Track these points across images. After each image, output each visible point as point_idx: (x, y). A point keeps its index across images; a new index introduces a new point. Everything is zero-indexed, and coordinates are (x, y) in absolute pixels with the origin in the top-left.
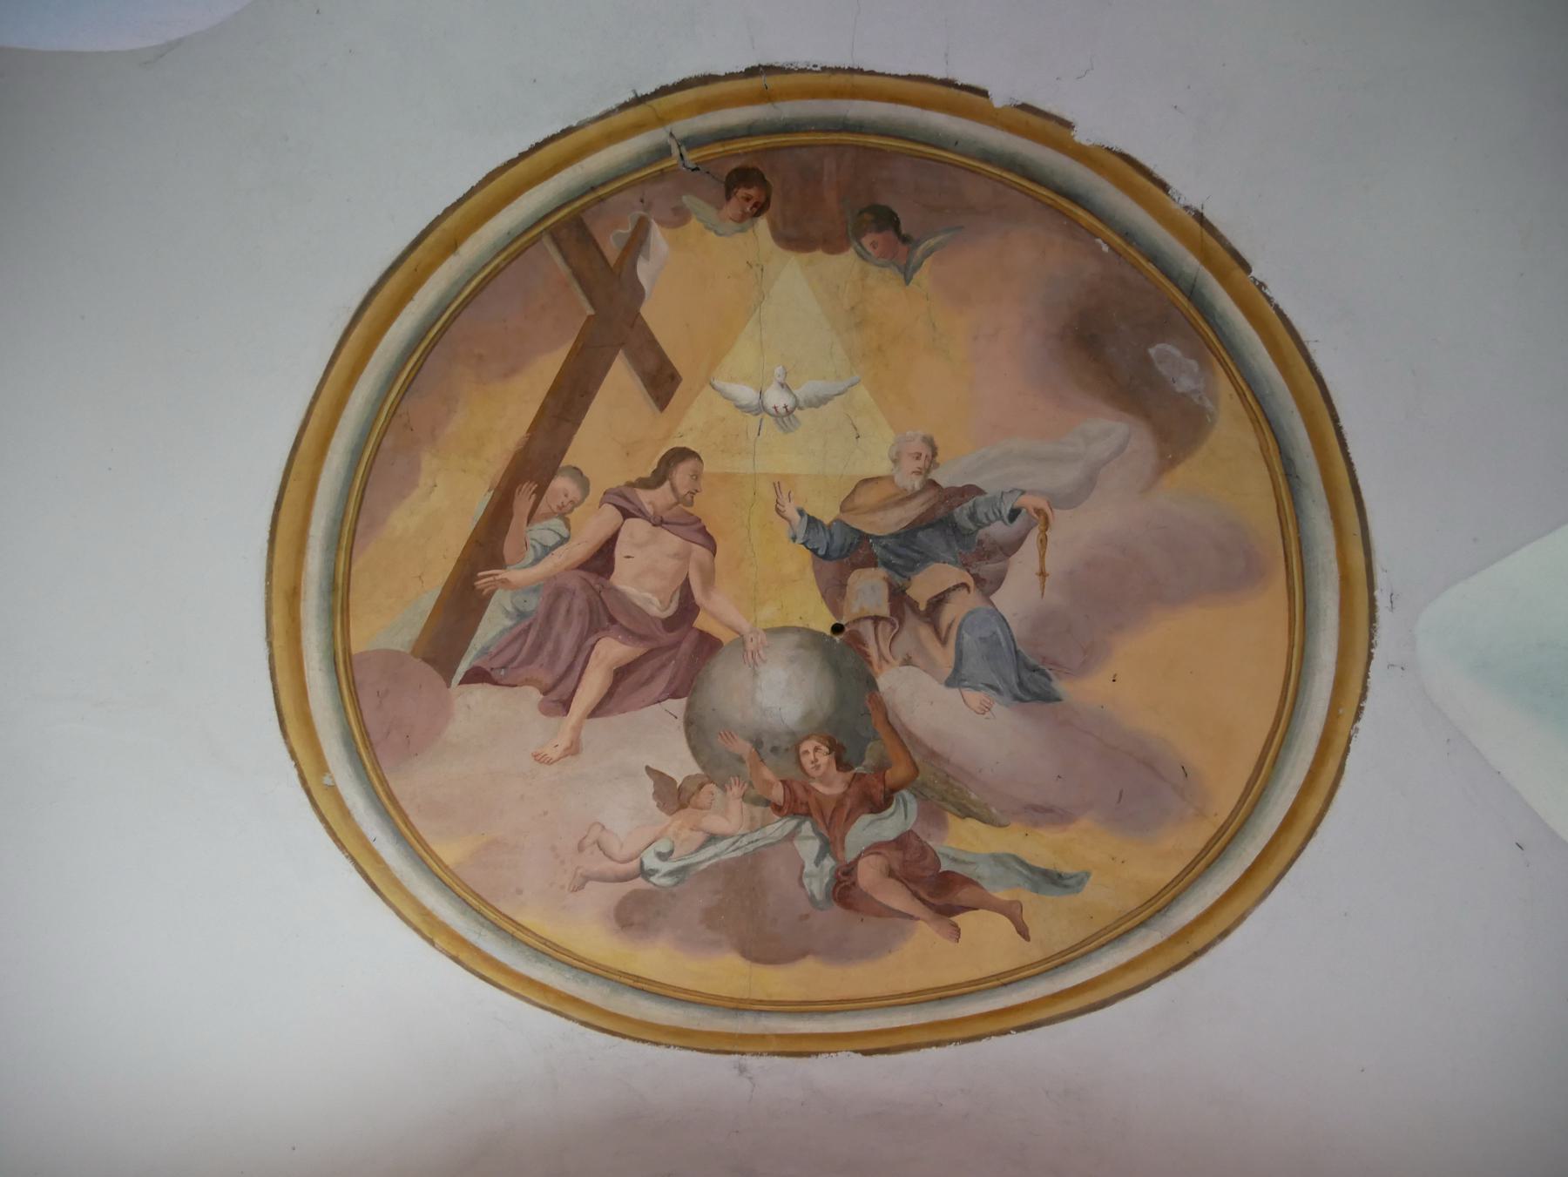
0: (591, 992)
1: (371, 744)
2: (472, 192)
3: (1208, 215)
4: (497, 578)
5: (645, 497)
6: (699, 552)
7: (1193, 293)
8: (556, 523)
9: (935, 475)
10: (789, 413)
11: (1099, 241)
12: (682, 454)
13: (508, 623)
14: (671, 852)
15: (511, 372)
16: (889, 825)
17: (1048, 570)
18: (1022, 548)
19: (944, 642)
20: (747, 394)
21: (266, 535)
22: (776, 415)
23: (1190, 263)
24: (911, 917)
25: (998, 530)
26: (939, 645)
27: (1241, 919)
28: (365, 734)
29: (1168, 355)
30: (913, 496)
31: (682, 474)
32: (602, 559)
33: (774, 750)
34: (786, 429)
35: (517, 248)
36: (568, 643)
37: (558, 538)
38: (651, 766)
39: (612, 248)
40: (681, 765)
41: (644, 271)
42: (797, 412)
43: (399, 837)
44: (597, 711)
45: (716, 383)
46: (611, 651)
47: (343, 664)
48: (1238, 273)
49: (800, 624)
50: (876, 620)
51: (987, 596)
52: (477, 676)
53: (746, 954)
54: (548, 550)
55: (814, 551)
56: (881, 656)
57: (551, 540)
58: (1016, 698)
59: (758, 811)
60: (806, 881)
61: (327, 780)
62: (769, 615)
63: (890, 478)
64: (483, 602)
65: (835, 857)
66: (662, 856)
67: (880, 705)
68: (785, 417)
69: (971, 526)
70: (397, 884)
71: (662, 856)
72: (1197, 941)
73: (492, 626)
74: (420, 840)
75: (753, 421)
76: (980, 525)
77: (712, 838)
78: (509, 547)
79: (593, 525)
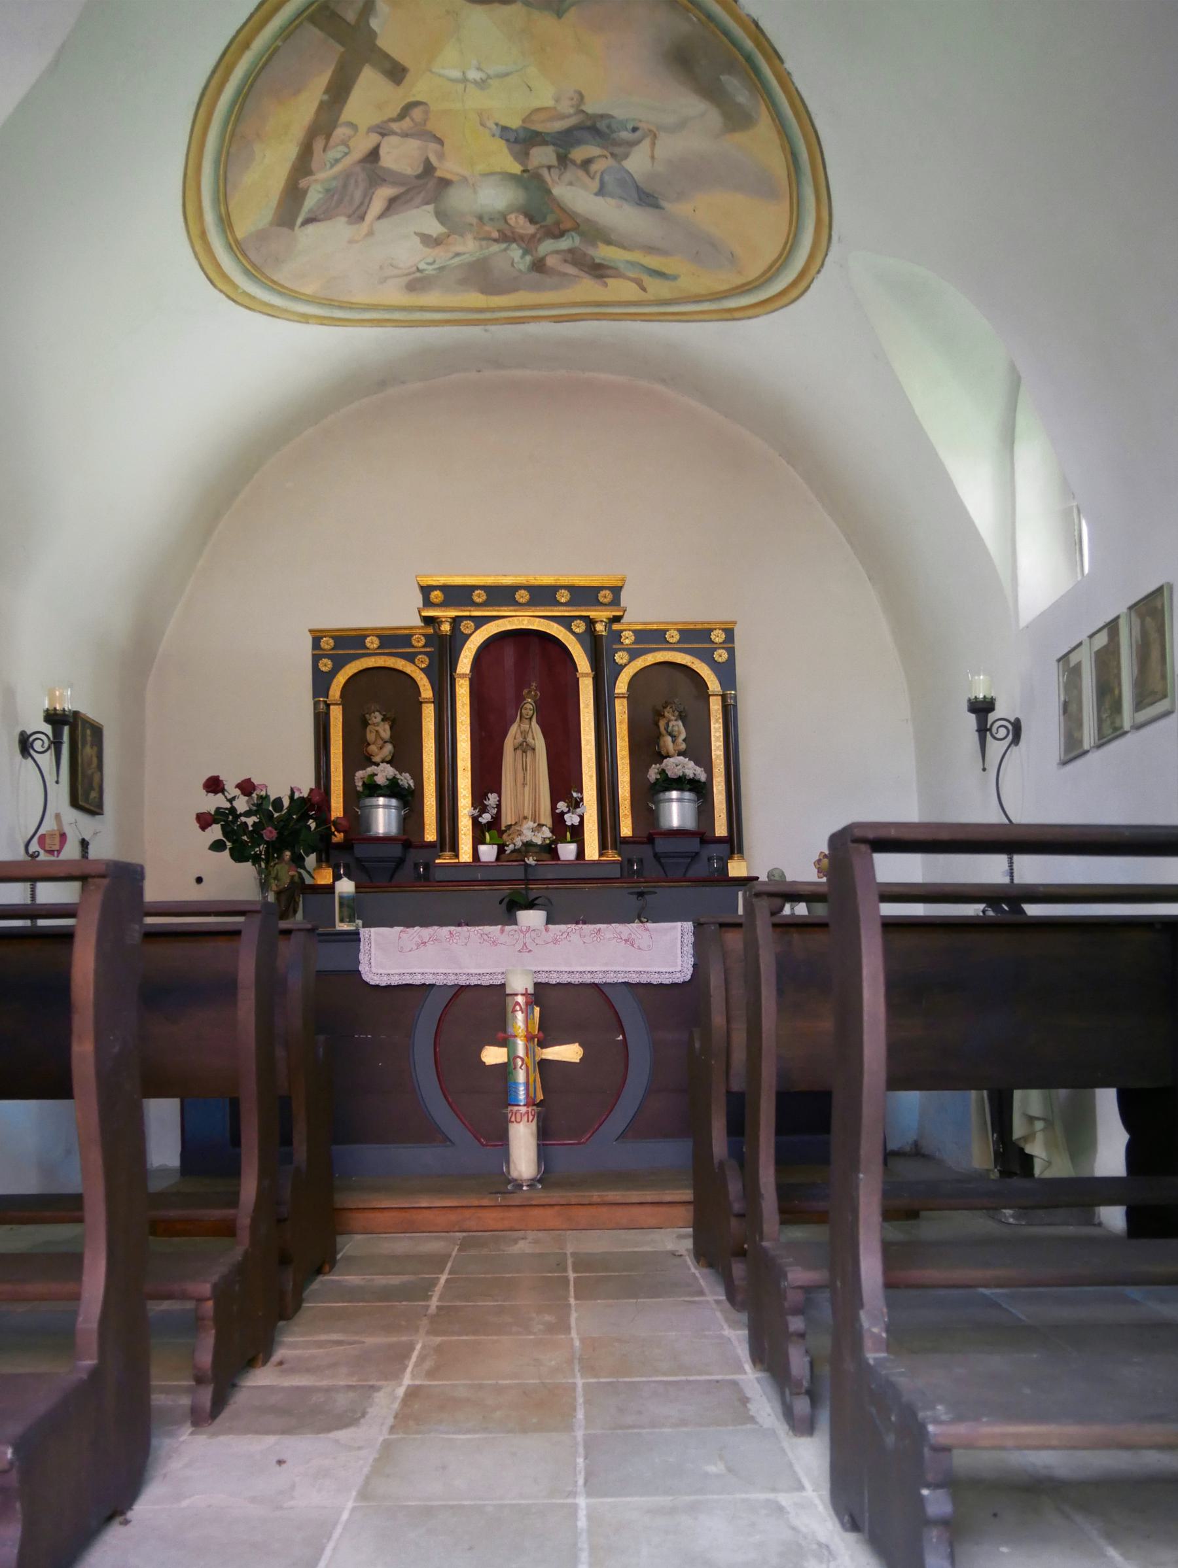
0: (397, 316)
1: (259, 269)
2: (252, 16)
3: (761, 24)
4: (505, 1253)
5: (395, 126)
6: (434, 146)
7: (749, 59)
8: (343, 148)
9: (584, 108)
10: (483, 81)
11: (691, 15)
12: (417, 104)
13: (321, 196)
14: (434, 261)
15: (297, 92)
16: (564, 244)
17: (656, 156)
18: (641, 145)
19: (593, 178)
20: (456, 74)
21: (181, 219)
22: (475, 82)
23: (749, 44)
24: (578, 277)
25: (625, 135)
26: (590, 180)
27: (757, 316)
28: (254, 265)
29: (731, 82)
30: (569, 116)
31: (417, 113)
32: (374, 155)
33: (491, 219)
34: (482, 89)
35: (287, 33)
36: (358, 195)
37: (343, 154)
38: (416, 231)
39: (351, 16)
40: (435, 228)
41: (374, 24)
42: (489, 81)
43: (281, 294)
44: (381, 216)
45: (434, 70)
46: (383, 194)
47: (237, 248)
48: (777, 62)
49: (499, 170)
50: (549, 168)
51: (619, 162)
52: (308, 221)
53: (482, 293)
54: (337, 161)
55: (507, 140)
56: (553, 180)
57: (339, 156)
58: (637, 204)
59: (484, 243)
60: (515, 265)
61: (240, 291)
62: (481, 167)
63: (555, 108)
64: (304, 193)
65: (532, 256)
66: (428, 264)
67: (554, 200)
68: (482, 84)
69: (607, 131)
70: (286, 311)
71: (428, 264)
72: (737, 315)
73: (312, 199)
74: (292, 290)
75: (460, 87)
76: (613, 132)
77: (458, 254)
78: (314, 165)
79: (362, 145)
